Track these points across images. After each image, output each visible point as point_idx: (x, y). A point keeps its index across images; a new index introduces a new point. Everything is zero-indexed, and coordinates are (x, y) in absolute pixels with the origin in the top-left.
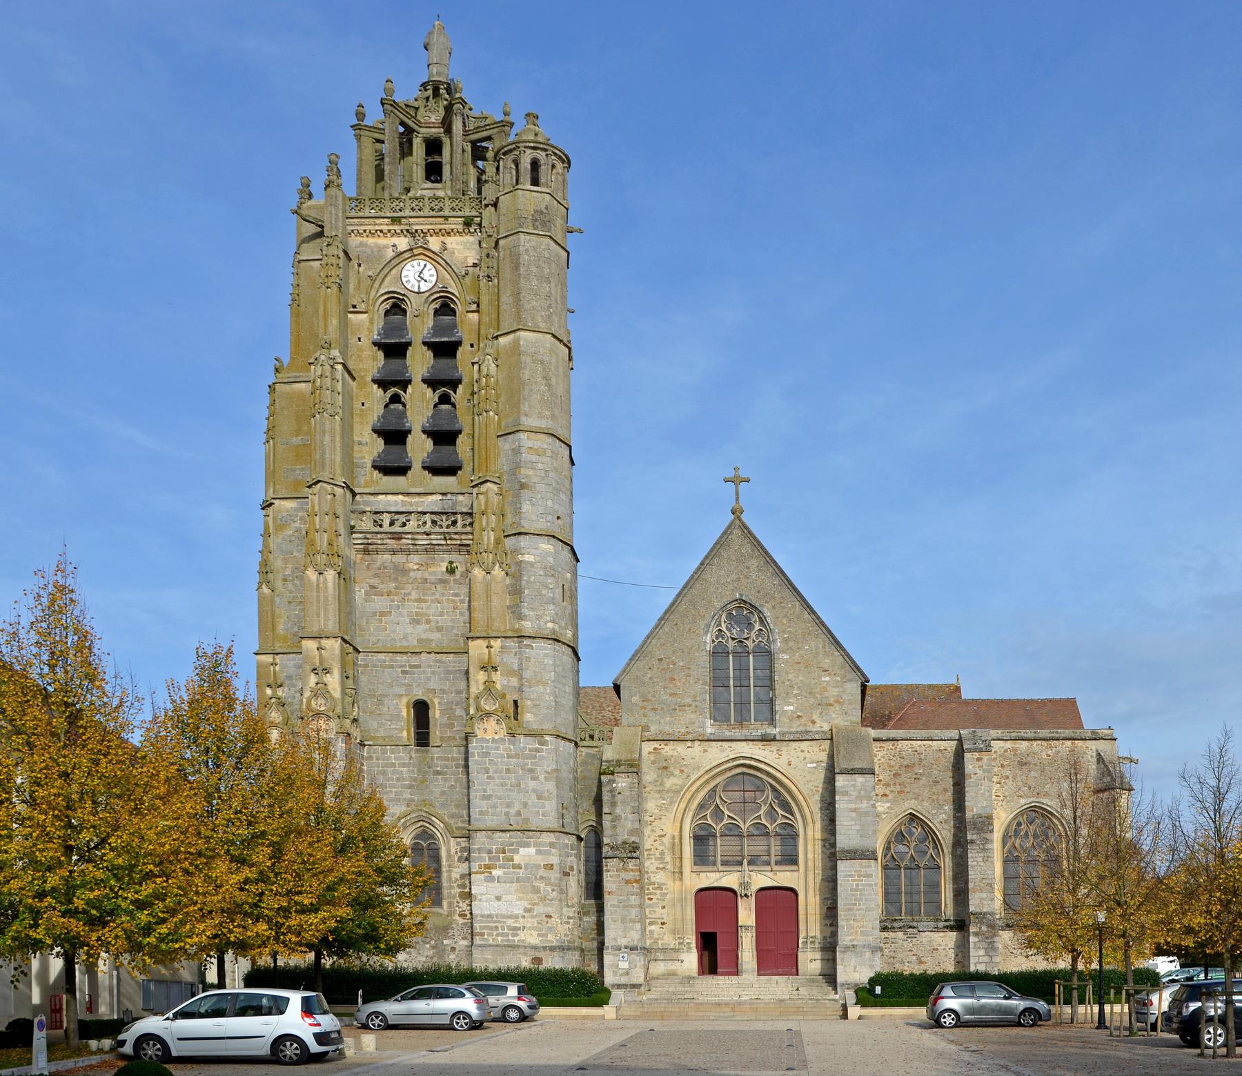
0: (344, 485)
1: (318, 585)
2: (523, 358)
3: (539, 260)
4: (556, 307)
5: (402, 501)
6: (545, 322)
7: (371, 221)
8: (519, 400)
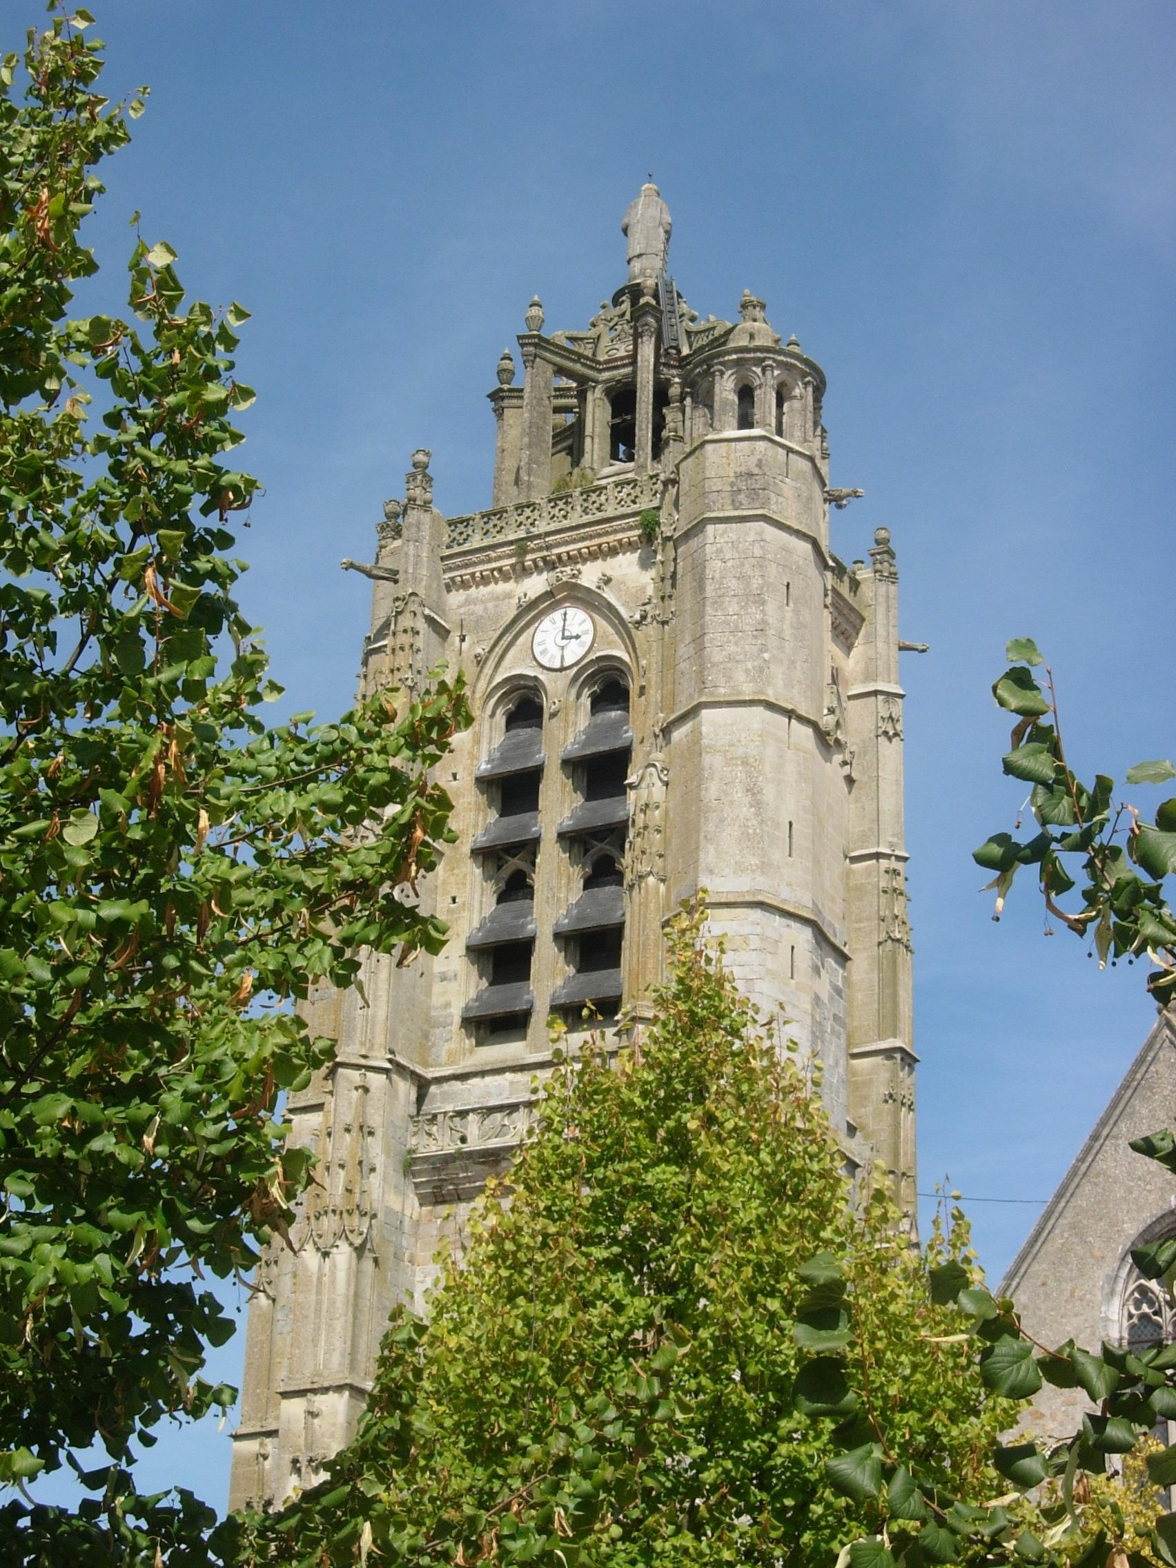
0: (388, 1066)
1: (320, 1276)
2: (707, 759)
3: (743, 565)
4: (781, 648)
5: (512, 1083)
6: (753, 680)
7: (481, 556)
8: (698, 842)
